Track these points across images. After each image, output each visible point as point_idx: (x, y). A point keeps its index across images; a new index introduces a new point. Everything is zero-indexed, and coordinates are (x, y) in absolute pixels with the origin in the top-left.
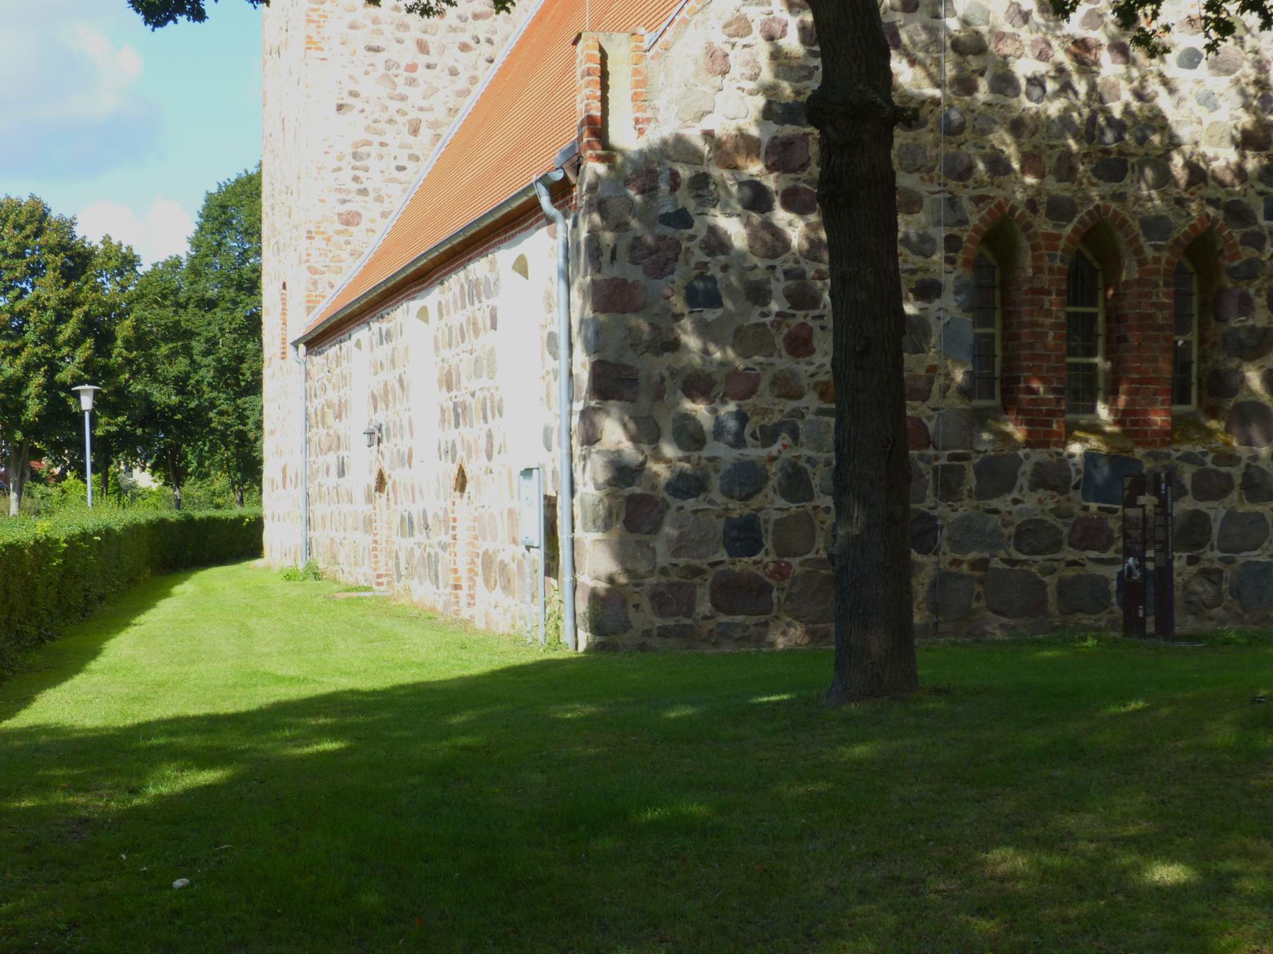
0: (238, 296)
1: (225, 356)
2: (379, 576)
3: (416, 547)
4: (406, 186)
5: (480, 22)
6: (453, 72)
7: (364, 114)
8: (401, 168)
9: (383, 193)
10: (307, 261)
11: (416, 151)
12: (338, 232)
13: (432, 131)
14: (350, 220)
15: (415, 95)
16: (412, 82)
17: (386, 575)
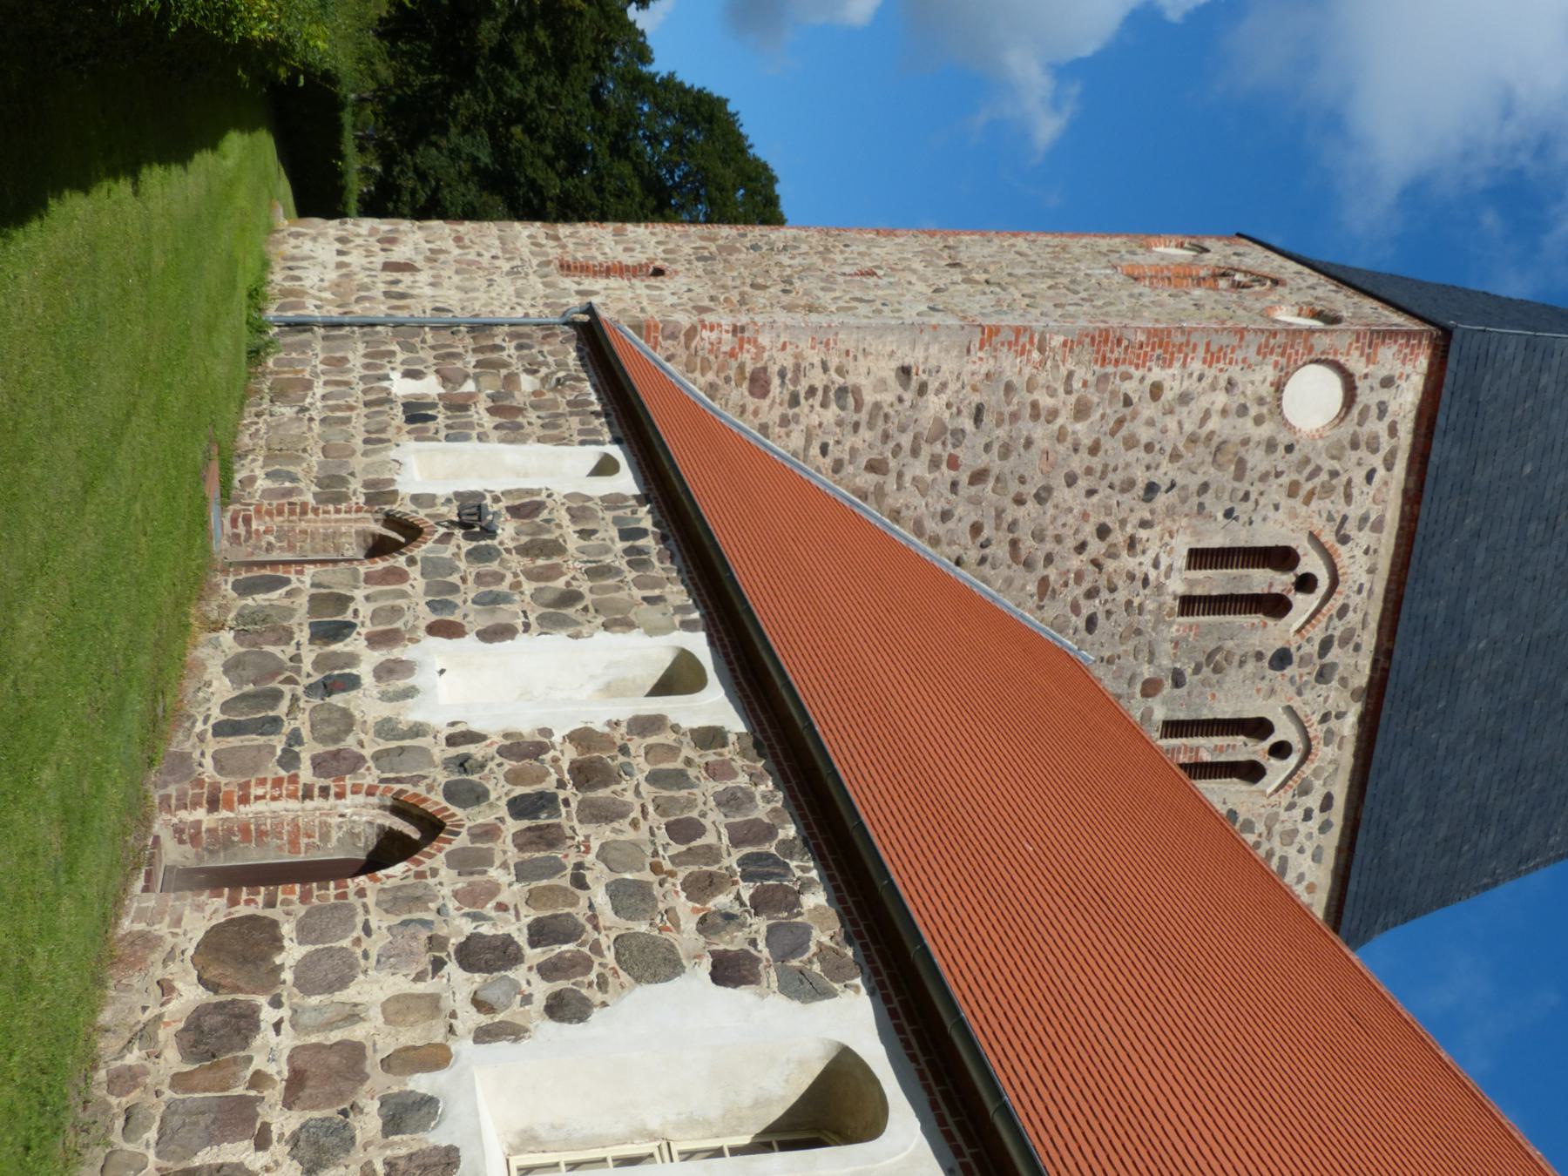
0: (608, 134)
1: (538, 117)
2: (247, 521)
3: (291, 650)
4: (801, 457)
5: (1007, 548)
6: (945, 516)
7: (896, 402)
8: (824, 450)
9: (793, 426)
10: (704, 326)
11: (850, 469)
12: (741, 367)
13: (872, 489)
14: (758, 384)
15: (919, 468)
16: (935, 463)
17: (249, 532)
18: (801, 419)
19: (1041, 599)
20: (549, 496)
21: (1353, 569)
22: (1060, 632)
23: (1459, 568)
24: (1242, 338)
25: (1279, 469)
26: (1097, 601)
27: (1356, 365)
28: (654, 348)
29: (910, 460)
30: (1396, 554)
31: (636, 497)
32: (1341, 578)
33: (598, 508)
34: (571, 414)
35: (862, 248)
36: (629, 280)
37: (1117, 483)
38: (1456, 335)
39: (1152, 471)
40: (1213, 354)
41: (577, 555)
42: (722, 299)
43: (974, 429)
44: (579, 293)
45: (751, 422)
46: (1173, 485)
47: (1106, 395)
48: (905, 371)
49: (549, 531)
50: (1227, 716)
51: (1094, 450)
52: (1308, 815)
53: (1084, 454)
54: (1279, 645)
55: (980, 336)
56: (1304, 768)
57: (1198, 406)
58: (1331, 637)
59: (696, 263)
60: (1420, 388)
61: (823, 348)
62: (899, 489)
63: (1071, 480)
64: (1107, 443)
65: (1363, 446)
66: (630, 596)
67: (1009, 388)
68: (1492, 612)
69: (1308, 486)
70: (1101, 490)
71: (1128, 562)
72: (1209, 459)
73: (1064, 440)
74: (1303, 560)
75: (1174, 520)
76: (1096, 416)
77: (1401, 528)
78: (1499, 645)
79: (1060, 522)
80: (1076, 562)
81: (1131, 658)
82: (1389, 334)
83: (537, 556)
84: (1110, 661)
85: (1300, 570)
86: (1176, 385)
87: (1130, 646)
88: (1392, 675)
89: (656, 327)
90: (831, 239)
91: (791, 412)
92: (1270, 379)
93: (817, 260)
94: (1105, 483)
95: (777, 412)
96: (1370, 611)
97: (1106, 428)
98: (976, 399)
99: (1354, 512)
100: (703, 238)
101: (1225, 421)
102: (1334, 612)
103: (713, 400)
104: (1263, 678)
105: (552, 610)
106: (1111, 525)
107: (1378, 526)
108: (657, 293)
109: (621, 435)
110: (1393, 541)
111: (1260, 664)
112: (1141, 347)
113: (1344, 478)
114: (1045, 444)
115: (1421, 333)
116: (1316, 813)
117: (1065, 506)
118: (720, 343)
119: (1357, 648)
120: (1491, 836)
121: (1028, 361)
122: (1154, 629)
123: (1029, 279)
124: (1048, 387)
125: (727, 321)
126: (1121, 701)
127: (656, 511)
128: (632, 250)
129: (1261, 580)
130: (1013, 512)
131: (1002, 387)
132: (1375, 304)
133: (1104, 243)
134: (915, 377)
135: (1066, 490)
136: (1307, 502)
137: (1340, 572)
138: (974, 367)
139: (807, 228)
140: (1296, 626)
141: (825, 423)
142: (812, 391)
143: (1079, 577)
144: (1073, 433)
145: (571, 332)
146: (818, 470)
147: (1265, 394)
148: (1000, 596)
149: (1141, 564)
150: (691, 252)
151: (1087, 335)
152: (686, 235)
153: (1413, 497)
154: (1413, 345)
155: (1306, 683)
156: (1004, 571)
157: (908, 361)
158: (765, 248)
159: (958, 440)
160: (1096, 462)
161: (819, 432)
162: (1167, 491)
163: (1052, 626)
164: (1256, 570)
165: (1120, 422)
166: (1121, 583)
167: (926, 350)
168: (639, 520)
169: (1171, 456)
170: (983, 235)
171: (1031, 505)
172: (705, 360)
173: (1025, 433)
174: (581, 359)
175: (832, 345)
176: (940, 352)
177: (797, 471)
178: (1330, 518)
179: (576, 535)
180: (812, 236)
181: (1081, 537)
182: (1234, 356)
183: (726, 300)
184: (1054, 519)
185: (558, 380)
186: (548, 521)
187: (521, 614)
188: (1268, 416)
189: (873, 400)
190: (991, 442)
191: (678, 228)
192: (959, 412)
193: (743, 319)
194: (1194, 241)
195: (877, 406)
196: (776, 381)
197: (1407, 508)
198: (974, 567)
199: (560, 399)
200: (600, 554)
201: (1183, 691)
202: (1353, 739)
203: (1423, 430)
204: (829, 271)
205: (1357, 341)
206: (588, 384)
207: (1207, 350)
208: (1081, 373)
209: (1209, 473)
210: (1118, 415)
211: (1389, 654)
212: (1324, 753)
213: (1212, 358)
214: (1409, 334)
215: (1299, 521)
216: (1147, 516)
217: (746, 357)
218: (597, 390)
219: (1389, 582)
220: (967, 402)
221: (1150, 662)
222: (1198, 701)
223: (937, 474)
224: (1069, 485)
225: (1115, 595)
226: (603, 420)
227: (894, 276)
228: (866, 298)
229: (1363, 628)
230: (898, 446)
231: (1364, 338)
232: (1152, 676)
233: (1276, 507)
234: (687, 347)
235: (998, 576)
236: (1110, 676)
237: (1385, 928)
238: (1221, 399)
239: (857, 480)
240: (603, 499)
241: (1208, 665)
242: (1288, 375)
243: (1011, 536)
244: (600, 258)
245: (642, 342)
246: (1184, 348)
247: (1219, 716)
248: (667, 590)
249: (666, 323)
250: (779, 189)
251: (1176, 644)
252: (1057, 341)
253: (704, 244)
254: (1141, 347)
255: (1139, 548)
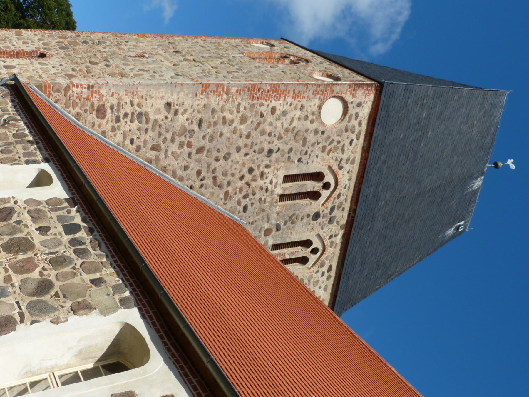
4: (122, 145)
5: (212, 180)
6: (186, 168)
7: (165, 119)
8: (132, 141)
9: (117, 131)
10: (74, 86)
11: (144, 150)
12: (92, 105)
13: (154, 158)
14: (101, 112)
15: (174, 148)
16: (181, 145)
18: (121, 128)
19: (225, 200)
20: (15, 203)
21: (343, 179)
22: (233, 213)
23: (378, 176)
24: (307, 88)
25: (319, 141)
26: (248, 199)
27: (349, 98)
28: (49, 97)
29: (170, 144)
30: (359, 172)
31: (67, 200)
32: (339, 183)
33: (47, 210)
34: (17, 143)
35: (134, 43)
36: (29, 59)
37: (257, 150)
38: (385, 85)
39: (271, 144)
40: (296, 95)
41: (42, 249)
42: (78, 70)
43: (198, 130)
44: (5, 67)
45: (98, 130)
46: (279, 150)
47: (254, 113)
48: (168, 105)
49: (21, 231)
50: (296, 240)
51: (248, 136)
52: (323, 274)
53: (244, 138)
54: (316, 211)
55: (201, 88)
56: (322, 257)
57: (289, 117)
58: (335, 206)
59: (60, 50)
60: (371, 107)
61: (131, 94)
62: (165, 157)
63: (238, 150)
64: (254, 133)
65: (349, 131)
66: (83, 280)
67: (213, 111)
68: (387, 190)
69: (329, 147)
70: (250, 153)
71: (261, 182)
72: (293, 138)
73: (236, 133)
74: (326, 177)
75: (279, 164)
76: (249, 122)
77: (361, 162)
78: (388, 202)
79: (233, 168)
80: (240, 184)
81: (261, 221)
82: (360, 85)
83: (17, 252)
84: (252, 223)
85: (325, 181)
86: (281, 108)
87: (260, 216)
88: (355, 219)
89: (49, 86)
90: (119, 38)
91: (116, 125)
92: (317, 104)
93: (115, 48)
94: (252, 150)
95: (110, 125)
96: (348, 195)
97: (253, 127)
98: (199, 116)
99: (345, 157)
100: (60, 38)
101: (300, 122)
102: (336, 196)
103: (79, 121)
104: (310, 224)
105: (35, 298)
106: (254, 168)
107: (353, 162)
108: (45, 67)
109: (48, 156)
110: (358, 167)
111: (309, 219)
112: (268, 92)
113: (342, 144)
114: (228, 135)
115: (372, 84)
116: (326, 273)
117: (236, 161)
118: (81, 93)
119: (343, 209)
120: (380, 271)
121: (222, 98)
122: (270, 209)
123: (211, 59)
124: (230, 110)
125: (84, 82)
126: (257, 238)
127: (81, 210)
128: (27, 43)
129: (311, 186)
130: (214, 164)
131: (211, 111)
132: (349, 71)
133: (234, 42)
134: (173, 107)
135: (236, 154)
136: (328, 154)
137: (339, 181)
138: (199, 102)
139: (106, 33)
140: (322, 203)
141: (132, 129)
142: (126, 115)
143: (241, 190)
144: (240, 129)
145: (7, 91)
146: (129, 151)
147: (315, 111)
148: (209, 201)
149: (265, 183)
150: (56, 44)
151: (246, 87)
152: (51, 36)
153: (366, 150)
154: (369, 90)
155: (325, 224)
156: (210, 190)
157: (170, 100)
158: (90, 42)
159: (191, 135)
160: (249, 142)
161: (130, 134)
162: (276, 152)
163: (229, 211)
164: (307, 181)
165: (259, 124)
166: (257, 191)
167: (178, 95)
168: (73, 218)
169: (278, 138)
170: (183, 37)
171: (222, 161)
172: (74, 102)
173: (220, 130)
174: (15, 107)
175: (135, 93)
176: (184, 96)
177: (119, 152)
178: (336, 160)
179: (38, 232)
180: (110, 36)
181: (242, 173)
182: (304, 95)
183: (80, 70)
184: (231, 166)
185: (5, 120)
186: (19, 222)
187: (16, 306)
188: (315, 120)
189: (154, 118)
190: (205, 135)
191: (46, 32)
192: (192, 122)
193: (92, 82)
194: (267, 41)
195: (156, 121)
196: (109, 111)
197: (363, 154)
198: (198, 189)
199: (8, 133)
200: (56, 246)
201: (280, 232)
202: (340, 244)
203: (371, 123)
204: (123, 55)
205: (350, 88)
206: (22, 122)
207: (294, 93)
208: (243, 104)
209: (293, 144)
210: (258, 121)
211: (355, 211)
212: (330, 250)
213: (296, 96)
214: (368, 85)
215: (325, 161)
216: (268, 163)
217: (95, 100)
218: (28, 127)
219: (356, 183)
220: (195, 118)
221: (268, 222)
222: (285, 236)
223: (182, 150)
224: (238, 152)
225: (255, 196)
226: (35, 146)
227: (153, 58)
228: (146, 69)
229: (346, 202)
230: (165, 138)
231: (352, 87)
232: (269, 227)
233: (317, 157)
234: (65, 96)
235: (207, 192)
236: (252, 229)
237: (346, 310)
238: (298, 113)
239: (147, 154)
240: (48, 202)
241: (289, 221)
242: (324, 102)
243: (213, 175)
244: (12, 47)
245: (43, 94)
246: (285, 92)
247: (293, 241)
248: (104, 273)
249: (54, 84)
250: (72, 9)
251: (278, 214)
252: (234, 90)
253: (61, 40)
254: (268, 92)
255: (265, 176)
